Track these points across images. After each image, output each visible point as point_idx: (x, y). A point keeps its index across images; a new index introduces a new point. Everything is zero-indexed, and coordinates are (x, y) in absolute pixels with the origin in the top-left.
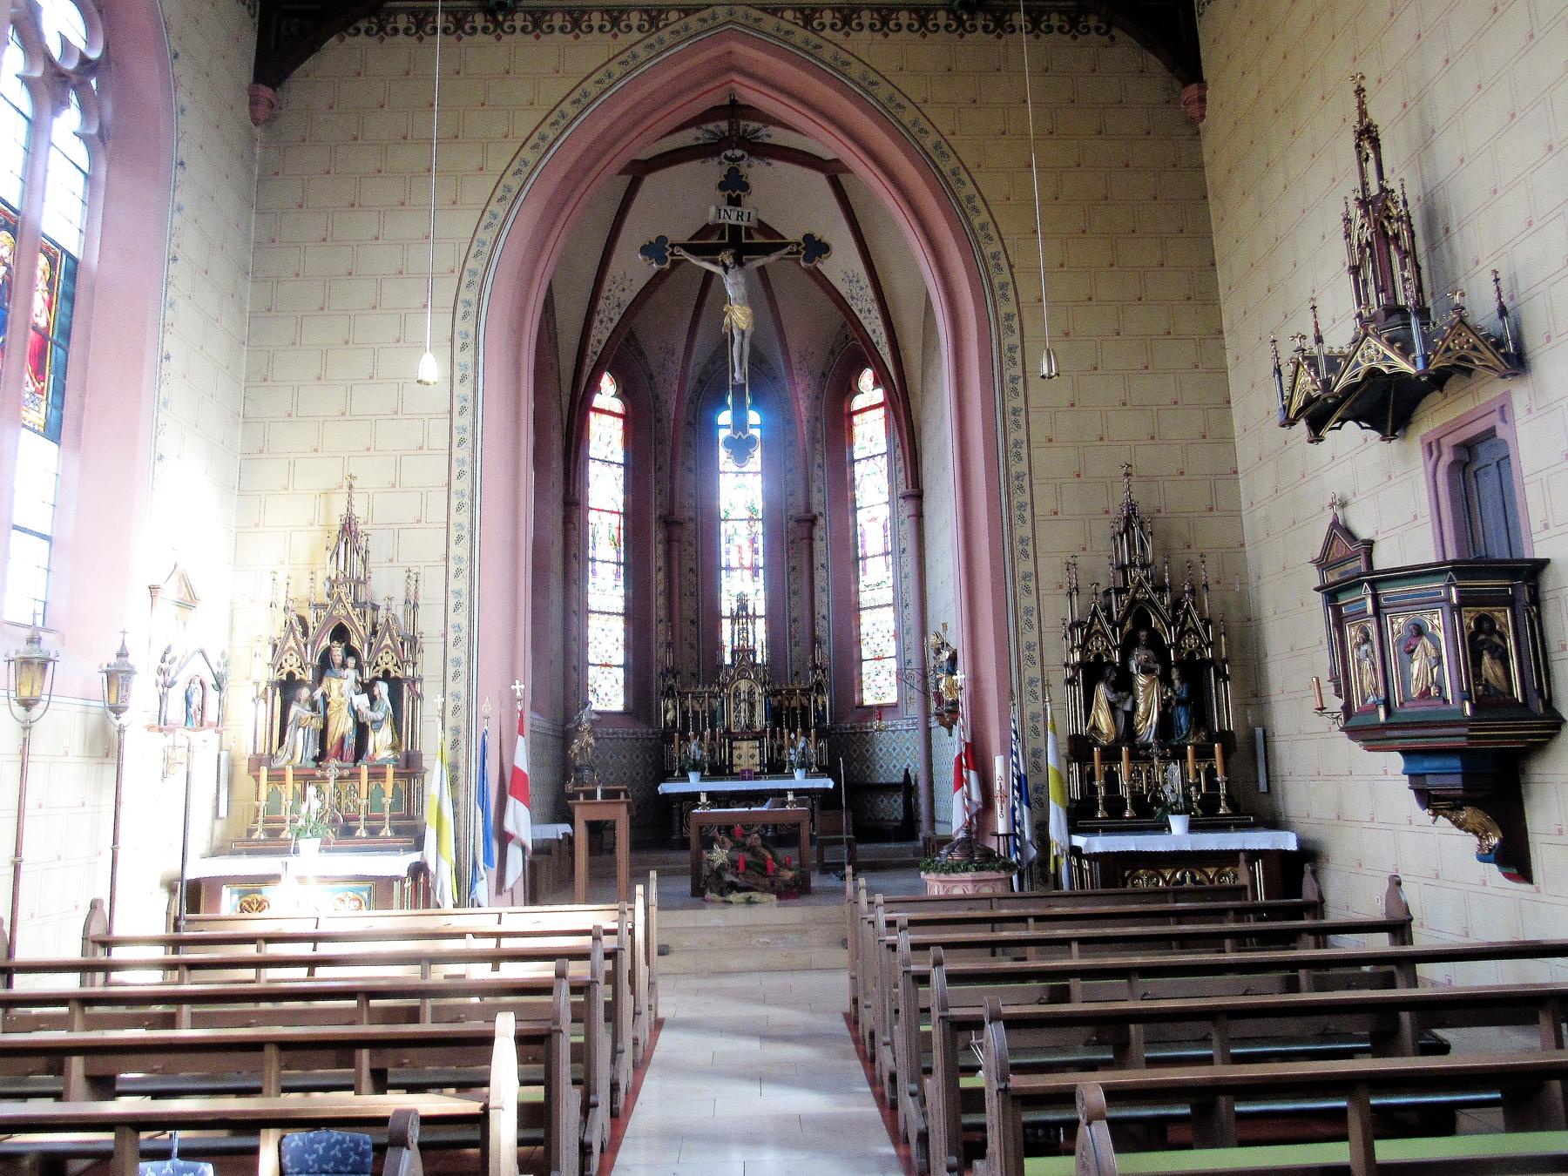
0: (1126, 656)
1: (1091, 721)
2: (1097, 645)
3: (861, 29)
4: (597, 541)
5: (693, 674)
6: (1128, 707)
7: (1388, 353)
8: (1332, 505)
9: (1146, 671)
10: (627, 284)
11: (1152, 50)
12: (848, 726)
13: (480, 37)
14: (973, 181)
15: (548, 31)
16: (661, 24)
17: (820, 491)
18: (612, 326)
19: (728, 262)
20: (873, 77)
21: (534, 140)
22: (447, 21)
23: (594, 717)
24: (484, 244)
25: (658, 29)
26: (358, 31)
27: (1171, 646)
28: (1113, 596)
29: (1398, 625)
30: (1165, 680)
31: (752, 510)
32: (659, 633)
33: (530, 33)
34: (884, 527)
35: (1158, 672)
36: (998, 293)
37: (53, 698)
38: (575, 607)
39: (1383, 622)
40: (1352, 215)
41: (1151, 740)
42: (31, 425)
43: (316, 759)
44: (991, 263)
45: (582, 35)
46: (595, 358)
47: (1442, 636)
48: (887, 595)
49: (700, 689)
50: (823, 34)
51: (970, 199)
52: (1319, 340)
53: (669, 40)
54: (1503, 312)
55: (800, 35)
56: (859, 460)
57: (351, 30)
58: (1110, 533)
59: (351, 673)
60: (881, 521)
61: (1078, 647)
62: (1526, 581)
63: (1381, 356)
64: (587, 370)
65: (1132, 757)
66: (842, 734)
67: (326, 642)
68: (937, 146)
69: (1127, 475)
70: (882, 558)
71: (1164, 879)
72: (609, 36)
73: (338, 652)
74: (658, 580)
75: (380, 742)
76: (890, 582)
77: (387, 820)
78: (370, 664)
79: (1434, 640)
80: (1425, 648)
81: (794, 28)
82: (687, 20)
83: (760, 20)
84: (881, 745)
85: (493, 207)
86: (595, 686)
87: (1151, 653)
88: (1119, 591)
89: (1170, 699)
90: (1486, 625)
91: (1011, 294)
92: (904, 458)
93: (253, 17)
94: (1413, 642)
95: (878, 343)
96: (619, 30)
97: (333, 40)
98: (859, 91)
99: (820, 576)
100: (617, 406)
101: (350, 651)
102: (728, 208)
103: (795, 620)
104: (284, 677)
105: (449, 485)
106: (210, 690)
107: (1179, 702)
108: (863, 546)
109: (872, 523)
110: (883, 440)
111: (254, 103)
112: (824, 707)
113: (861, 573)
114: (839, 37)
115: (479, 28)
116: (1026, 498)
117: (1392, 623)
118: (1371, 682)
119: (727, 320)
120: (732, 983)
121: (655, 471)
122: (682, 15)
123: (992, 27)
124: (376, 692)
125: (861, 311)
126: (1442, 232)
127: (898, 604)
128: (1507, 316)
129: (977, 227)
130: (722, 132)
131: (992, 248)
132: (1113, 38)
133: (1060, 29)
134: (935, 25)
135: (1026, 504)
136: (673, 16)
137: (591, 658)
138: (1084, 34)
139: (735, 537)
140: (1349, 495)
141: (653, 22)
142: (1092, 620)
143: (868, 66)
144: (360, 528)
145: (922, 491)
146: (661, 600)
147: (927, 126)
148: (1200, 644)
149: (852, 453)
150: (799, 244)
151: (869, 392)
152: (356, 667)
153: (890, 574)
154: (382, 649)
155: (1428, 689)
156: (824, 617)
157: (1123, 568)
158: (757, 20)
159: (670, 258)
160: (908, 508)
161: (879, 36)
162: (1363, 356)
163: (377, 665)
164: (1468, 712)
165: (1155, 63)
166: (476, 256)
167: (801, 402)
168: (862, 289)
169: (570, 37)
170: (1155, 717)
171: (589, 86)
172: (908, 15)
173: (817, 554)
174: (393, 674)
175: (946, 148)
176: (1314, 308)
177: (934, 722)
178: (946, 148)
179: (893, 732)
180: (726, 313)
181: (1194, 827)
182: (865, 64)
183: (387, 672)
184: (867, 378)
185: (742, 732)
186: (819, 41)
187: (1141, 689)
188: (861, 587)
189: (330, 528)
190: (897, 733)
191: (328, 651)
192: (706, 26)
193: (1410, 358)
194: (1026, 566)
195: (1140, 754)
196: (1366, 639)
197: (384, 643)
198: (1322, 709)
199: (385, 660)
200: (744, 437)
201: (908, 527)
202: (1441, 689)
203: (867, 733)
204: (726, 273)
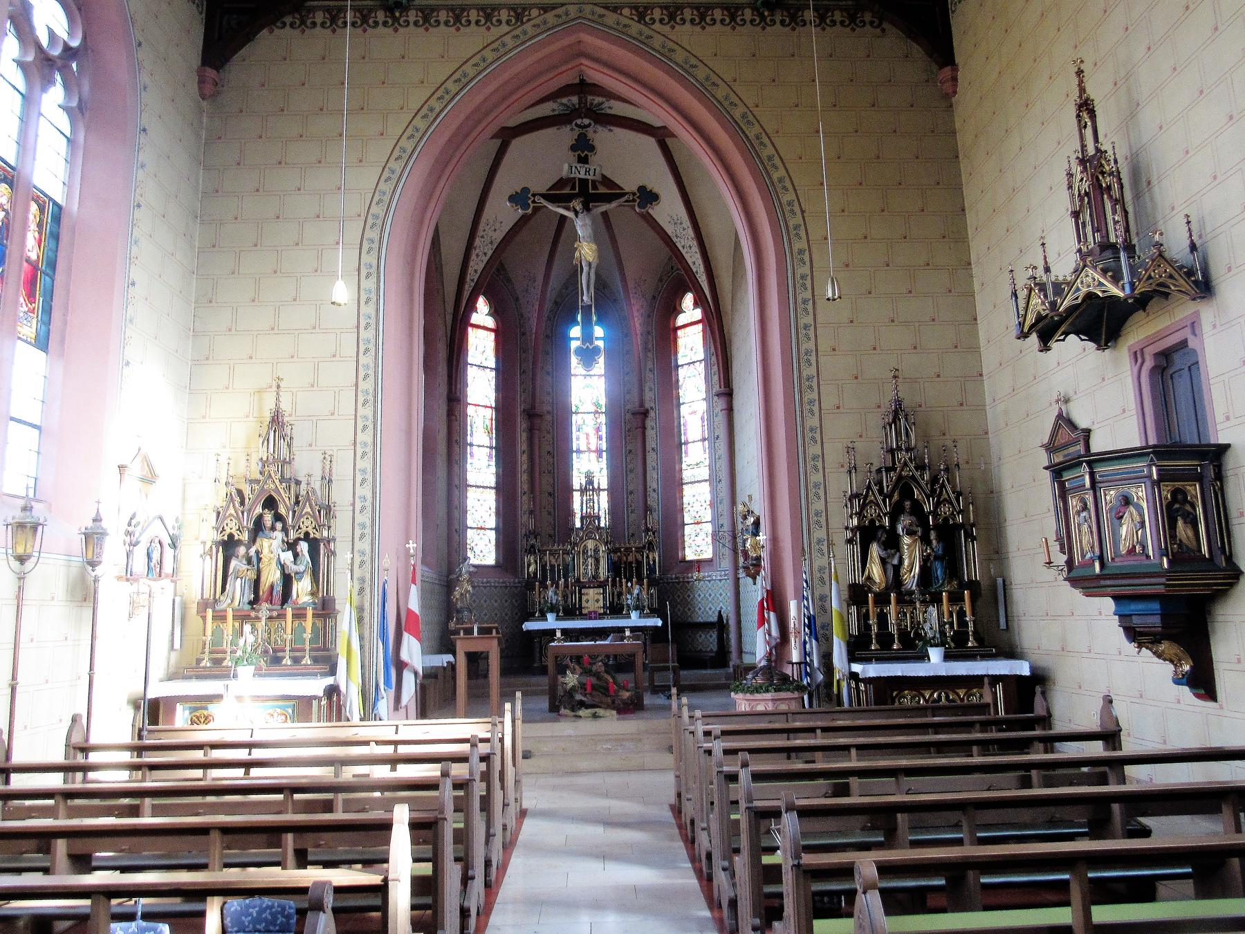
0: (894, 521)
2: (871, 512)
3: (684, 23)
4: (474, 430)
5: (550, 536)
6: (895, 562)
9: (910, 533)
10: (497, 226)
11: (915, 39)
12: (674, 576)
13: (381, 29)
14: (772, 143)
15: (435, 24)
17: (651, 390)
18: (486, 259)
19: (578, 208)
20: (693, 61)
21: (424, 111)
22: (355, 17)
23: (472, 569)
24: (384, 193)
25: (522, 23)
26: (284, 25)
27: (930, 513)
28: (884, 474)
29: (1110, 496)
30: (925, 540)
31: (597, 405)
32: (524, 503)
33: (421, 26)
34: (702, 419)
35: (920, 534)
36: (793, 233)
38: (456, 482)
39: (1098, 494)
40: (1074, 171)
41: (914, 588)
42: (25, 338)
44: (787, 209)
45: (462, 28)
46: (473, 284)
47: (1145, 505)
48: (704, 473)
49: (555, 547)
50: (653, 27)
51: (770, 158)
52: (1047, 270)
53: (531, 32)
54: (1193, 247)
55: (635, 28)
56: (682, 365)
57: (279, 24)
58: (881, 423)
60: (700, 414)
61: (856, 514)
62: (1212, 462)
63: (1096, 283)
64: (466, 294)
66: (668, 583)
67: (259, 510)
68: (744, 116)
69: (895, 377)
70: (701, 443)
71: (924, 698)
72: (483, 29)
74: (522, 461)
75: (302, 589)
76: (707, 462)
77: (307, 651)
78: (294, 527)
79: (1139, 508)
80: (1131, 515)
81: (630, 22)
82: (545, 16)
83: (603, 16)
84: (699, 592)
85: (392, 164)
86: (473, 545)
87: (914, 519)
88: (888, 470)
89: (929, 555)
90: (1180, 497)
91: (803, 233)
92: (718, 364)
93: (201, 13)
94: (1122, 510)
95: (697, 272)
96: (492, 24)
97: (265, 32)
98: (682, 73)
99: (651, 457)
100: (490, 322)
101: (278, 517)
102: (578, 165)
103: (631, 493)
104: (226, 538)
105: (357, 385)
106: (167, 548)
107: (936, 558)
108: (685, 434)
109: (693, 415)
110: (701, 350)
111: (201, 82)
112: (654, 561)
113: (683, 455)
114: (666, 29)
115: (381, 22)
116: (815, 396)
117: (1105, 495)
118: (1089, 542)
119: (577, 254)
120: (581, 780)
121: (520, 374)
122: (542, 12)
123: (787, 21)
124: (299, 550)
125: (683, 247)
126: (1145, 184)
127: (713, 480)
128: (1196, 251)
129: (775, 180)
130: (574, 105)
131: (787, 197)
132: (883, 30)
133: (842, 23)
134: (742, 20)
135: (815, 400)
136: (535, 12)
137: (469, 523)
138: (861, 27)
139: (584, 426)
140: (1071, 393)
141: (519, 17)
143: (690, 52)
144: (286, 419)
145: (732, 390)
146: (525, 477)
147: (736, 100)
149: (676, 360)
150: (634, 194)
151: (690, 312)
153: (707, 456)
154: (303, 516)
155: (1134, 547)
156: (654, 490)
157: (891, 451)
158: (601, 16)
159: (532, 205)
160: (721, 404)
161: (698, 29)
162: (1082, 283)
163: (299, 528)
164: (1166, 566)
165: (917, 50)
166: (378, 203)
168: (684, 229)
169: (453, 29)
170: (917, 569)
171: (468, 68)
172: (721, 12)
173: (648, 440)
174: (312, 536)
175: (751, 118)
176: (1043, 244)
177: (742, 574)
178: (751, 118)
179: (709, 581)
180: (576, 249)
181: (948, 657)
182: (687, 51)
183: (307, 534)
184: (688, 300)
186: (651, 33)
188: (684, 466)
189: (262, 419)
190: (712, 582)
191: (260, 517)
192: (560, 21)
193: (1120, 284)
194: (814, 450)
195: (905, 599)
196: (1085, 508)
197: (305, 510)
198: (1050, 563)
199: (305, 524)
200: (591, 347)
201: (721, 419)
202: (1144, 547)
203: (688, 582)
204: (577, 217)
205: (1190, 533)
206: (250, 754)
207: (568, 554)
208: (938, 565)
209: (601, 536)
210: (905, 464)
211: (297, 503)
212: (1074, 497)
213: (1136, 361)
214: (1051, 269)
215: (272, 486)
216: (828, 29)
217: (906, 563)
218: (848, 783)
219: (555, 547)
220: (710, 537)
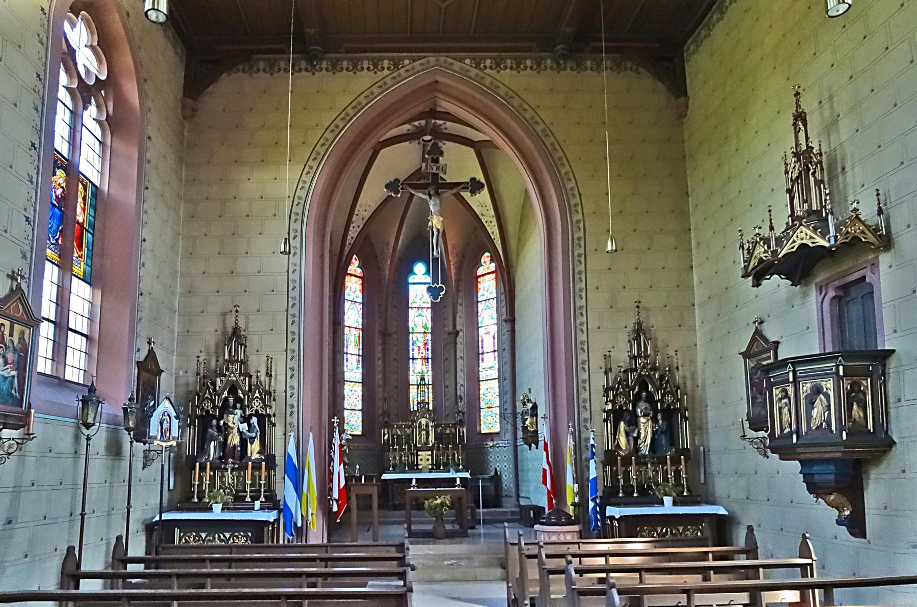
0: (634, 407)
1: (616, 442)
2: (621, 400)
4: (349, 343)
6: (635, 435)
7: (813, 235)
8: (755, 322)
11: (659, 79)
12: (474, 444)
13: (303, 73)
16: (400, 66)
18: (359, 230)
19: (431, 193)
20: (511, 93)
23: (350, 437)
24: (305, 182)
25: (399, 69)
27: (658, 401)
28: (629, 374)
29: (806, 388)
30: (655, 420)
31: (425, 327)
32: (379, 393)
34: (494, 337)
35: (651, 415)
36: (573, 209)
37: (101, 425)
38: (338, 378)
39: (798, 386)
40: (788, 162)
41: (647, 453)
42: (76, 274)
43: (220, 458)
46: (350, 247)
47: (831, 393)
48: (495, 374)
50: (485, 71)
51: (560, 159)
52: (772, 228)
53: (404, 75)
54: (880, 211)
55: (474, 71)
56: (481, 301)
57: (234, 70)
58: (627, 339)
59: (239, 412)
60: (492, 335)
61: (611, 401)
62: (880, 363)
63: (808, 237)
65: (637, 464)
69: (638, 307)
71: (657, 532)
72: (372, 73)
73: (231, 400)
75: (254, 449)
76: (497, 366)
77: (248, 493)
78: (248, 407)
79: (827, 396)
80: (821, 400)
84: (491, 455)
85: (310, 163)
87: (647, 405)
88: (632, 370)
89: (657, 430)
90: (856, 388)
94: (815, 397)
98: (504, 102)
99: (460, 363)
100: (359, 272)
101: (238, 400)
102: (432, 164)
103: (447, 387)
104: (204, 413)
105: (287, 311)
106: (173, 419)
107: (662, 432)
108: (482, 347)
110: (494, 291)
111: (184, 107)
112: (463, 433)
113: (481, 361)
116: (584, 319)
117: (803, 386)
118: (788, 420)
119: (430, 224)
120: (437, 587)
124: (251, 422)
125: (486, 222)
126: (840, 169)
127: (501, 378)
128: (883, 214)
130: (422, 126)
135: (584, 323)
136: (406, 62)
137: (346, 406)
139: (417, 342)
140: (765, 318)
141: (396, 66)
142: (618, 386)
145: (515, 318)
146: (380, 376)
147: (539, 120)
148: (626, 401)
150: (468, 183)
151: (487, 265)
152: (240, 409)
153: (496, 362)
155: (821, 424)
156: (462, 385)
157: (635, 358)
159: (401, 191)
160: (507, 327)
161: (515, 72)
162: (797, 237)
163: (252, 407)
164: (844, 438)
165: (660, 86)
167: (452, 270)
168: (488, 210)
170: (649, 441)
174: (260, 412)
175: (548, 132)
176: (770, 211)
177: (520, 442)
178: (548, 132)
179: (498, 447)
180: (429, 220)
181: (675, 503)
183: (257, 411)
184: (486, 257)
187: (642, 425)
188: (481, 369)
191: (226, 399)
192: (424, 67)
193: (827, 238)
195: (641, 462)
196: (786, 396)
197: (256, 395)
198: (744, 436)
199: (256, 405)
202: (829, 425)
204: (431, 198)
205: (862, 414)
206: (580, 563)
207: (409, 428)
208: (663, 437)
209: (430, 416)
210: (644, 367)
211: (250, 389)
212: (848, 380)
213: (821, 294)
214: (775, 228)
217: (642, 435)
218: (61, 588)
219: (400, 423)
220: (498, 417)
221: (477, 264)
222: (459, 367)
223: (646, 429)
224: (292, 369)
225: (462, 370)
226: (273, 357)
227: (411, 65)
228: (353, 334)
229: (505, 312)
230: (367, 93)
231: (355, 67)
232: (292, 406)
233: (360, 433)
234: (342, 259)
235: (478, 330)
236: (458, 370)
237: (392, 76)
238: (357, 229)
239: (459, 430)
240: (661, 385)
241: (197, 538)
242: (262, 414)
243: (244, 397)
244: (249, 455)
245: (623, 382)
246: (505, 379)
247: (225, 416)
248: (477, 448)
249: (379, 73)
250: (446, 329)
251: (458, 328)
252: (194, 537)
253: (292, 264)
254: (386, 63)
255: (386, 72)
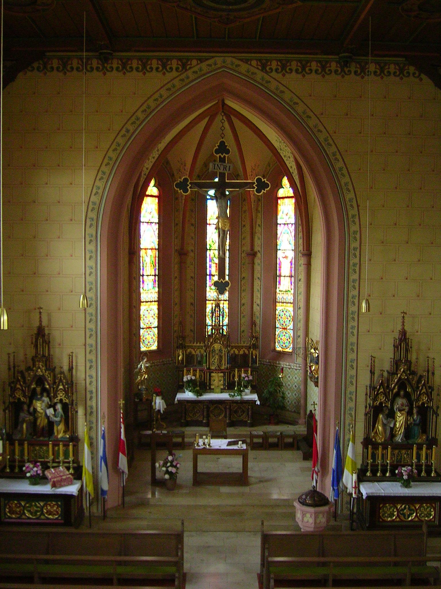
3: (132, 70)
4: (145, 265)
6: (392, 426)
9: (400, 411)
14: (343, 160)
15: (149, 70)
16: (188, 67)
17: (259, 239)
21: (123, 132)
25: (186, 70)
26: (33, 68)
30: (410, 413)
34: (291, 263)
44: (348, 204)
46: (145, 177)
48: (290, 297)
49: (195, 344)
50: (271, 74)
51: (341, 169)
53: (192, 77)
55: (260, 75)
57: (30, 68)
60: (289, 259)
66: (264, 364)
73: (39, 389)
75: (60, 431)
76: (292, 291)
81: (256, 71)
82: (201, 65)
83: (239, 65)
85: (103, 168)
86: (144, 339)
89: (411, 424)
91: (357, 220)
92: (303, 231)
95: (293, 173)
97: (21, 74)
99: (257, 283)
101: (44, 390)
102: (219, 164)
103: (244, 304)
104: (16, 401)
108: (280, 270)
109: (285, 259)
112: (256, 357)
113: (278, 283)
114: (279, 76)
115: (95, 68)
116: (355, 324)
121: (174, 227)
122: (199, 62)
123: (359, 72)
125: (285, 156)
131: (350, 196)
132: (421, 80)
136: (194, 62)
138: (406, 77)
141: (184, 66)
143: (294, 93)
146: (177, 294)
154: (59, 391)
158: (238, 66)
159: (189, 190)
160: (303, 261)
166: (95, 194)
169: (141, 74)
171: (150, 102)
173: (256, 272)
178: (331, 142)
182: (293, 92)
184: (285, 181)
185: (216, 370)
188: (278, 290)
190: (291, 369)
194: (352, 356)
200: (224, 282)
201: (302, 269)
203: (276, 366)
211: (55, 383)
215: (41, 374)
216: (385, 78)
221: (277, 186)
222: (256, 287)
223: (400, 419)
224: (91, 361)
225: (258, 291)
226: (74, 351)
227: (198, 66)
228: (149, 256)
229: (302, 244)
230: (156, 96)
231: (144, 66)
232: (91, 392)
233: (154, 347)
234: (137, 191)
235: (277, 252)
236: (255, 290)
237: (181, 77)
238: (153, 159)
239: (252, 352)
240: (418, 387)
241: (18, 505)
242: (66, 403)
243: (51, 389)
244: (56, 434)
245: (385, 385)
246: (300, 308)
247: (34, 401)
248: (270, 365)
249: (167, 74)
250: (244, 248)
251: (256, 248)
252: (16, 504)
253: (89, 267)
254: (174, 64)
255: (175, 74)
